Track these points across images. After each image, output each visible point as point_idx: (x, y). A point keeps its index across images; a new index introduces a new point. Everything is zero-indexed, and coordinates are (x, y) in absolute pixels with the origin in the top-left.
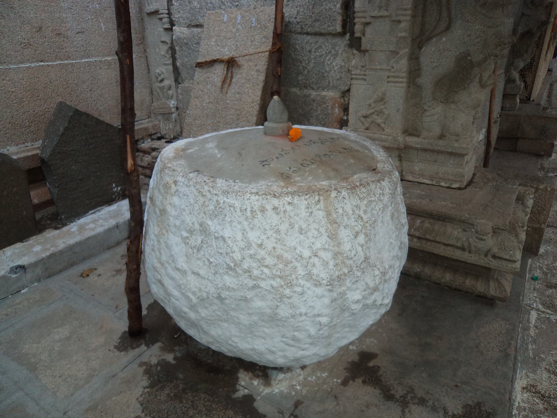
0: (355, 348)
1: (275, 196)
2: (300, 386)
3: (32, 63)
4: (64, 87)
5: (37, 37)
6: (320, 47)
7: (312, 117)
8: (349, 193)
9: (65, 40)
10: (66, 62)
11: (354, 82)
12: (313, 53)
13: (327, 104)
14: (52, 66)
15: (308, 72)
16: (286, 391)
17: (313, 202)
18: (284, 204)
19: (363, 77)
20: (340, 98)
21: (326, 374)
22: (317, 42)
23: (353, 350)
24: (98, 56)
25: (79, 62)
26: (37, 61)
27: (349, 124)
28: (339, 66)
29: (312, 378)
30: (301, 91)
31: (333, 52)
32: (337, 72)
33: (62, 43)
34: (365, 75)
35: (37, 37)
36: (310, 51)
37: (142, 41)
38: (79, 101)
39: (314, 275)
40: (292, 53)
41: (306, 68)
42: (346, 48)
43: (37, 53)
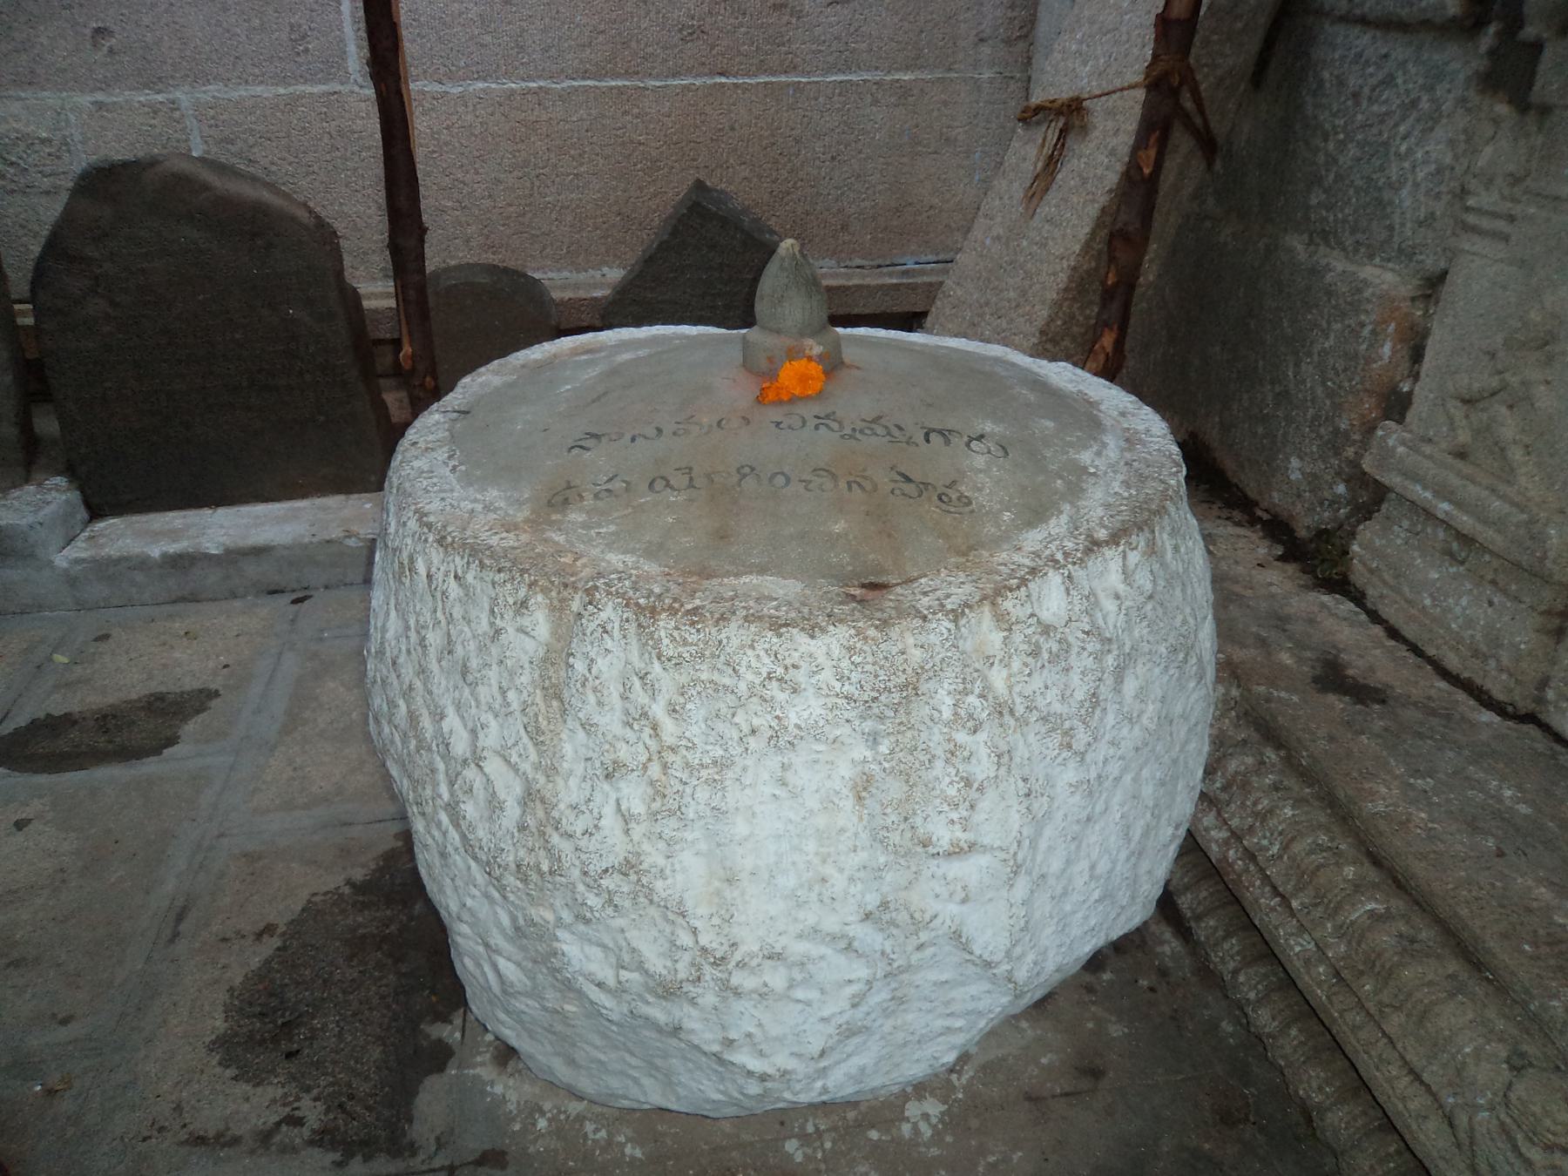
0: (799, 1158)
1: (441, 541)
2: (550, 1125)
3: (698, 75)
4: (764, 143)
5: (722, 11)
6: (1389, 81)
7: (1309, 354)
8: (627, 621)
9: (794, 21)
10: (783, 79)
11: (1467, 243)
12: (1365, 104)
13: (1363, 317)
14: (746, 88)
15: (1339, 178)
16: (512, 1108)
17: (511, 601)
18: (446, 574)
19: (1501, 225)
20: (1413, 299)
21: (638, 1153)
22: (1386, 56)
23: (790, 1157)
24: (877, 68)
25: (817, 82)
26: (712, 74)
27: (1409, 416)
28: (1433, 167)
29: (596, 1131)
30: (1312, 248)
31: (1425, 105)
32: (1423, 189)
33: (784, 29)
34: (1511, 219)
35: (722, 11)
36: (1356, 96)
37: (1025, 30)
38: (795, 183)
39: (464, 818)
40: (1308, 99)
41: (1336, 161)
42: (1471, 94)
43: (714, 52)
